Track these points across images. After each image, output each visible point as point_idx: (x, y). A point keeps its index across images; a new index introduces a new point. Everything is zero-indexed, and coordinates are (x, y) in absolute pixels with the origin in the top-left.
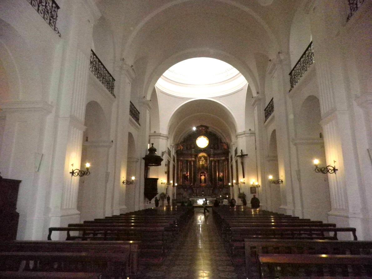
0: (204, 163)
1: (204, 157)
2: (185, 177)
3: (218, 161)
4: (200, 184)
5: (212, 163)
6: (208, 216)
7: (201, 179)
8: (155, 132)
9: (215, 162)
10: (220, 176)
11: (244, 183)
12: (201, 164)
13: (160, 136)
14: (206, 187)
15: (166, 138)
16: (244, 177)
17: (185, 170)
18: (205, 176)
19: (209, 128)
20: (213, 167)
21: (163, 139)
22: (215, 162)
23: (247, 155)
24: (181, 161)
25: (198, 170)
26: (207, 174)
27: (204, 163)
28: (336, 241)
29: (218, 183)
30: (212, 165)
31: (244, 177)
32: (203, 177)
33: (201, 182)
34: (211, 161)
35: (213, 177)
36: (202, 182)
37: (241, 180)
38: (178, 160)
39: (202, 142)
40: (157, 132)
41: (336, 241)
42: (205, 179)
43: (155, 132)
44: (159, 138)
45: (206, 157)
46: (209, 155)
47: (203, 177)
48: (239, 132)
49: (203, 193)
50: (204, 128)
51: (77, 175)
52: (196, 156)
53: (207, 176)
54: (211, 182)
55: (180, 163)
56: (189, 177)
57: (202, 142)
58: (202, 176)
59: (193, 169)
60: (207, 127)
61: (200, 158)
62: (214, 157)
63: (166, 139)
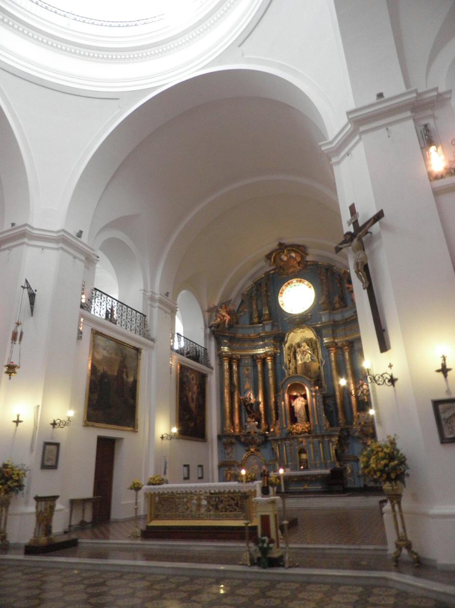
1: (309, 342)
2: (249, 409)
4: (289, 426)
6: (42, 581)
7: (292, 408)
8: (13, 224)
9: (339, 349)
11: (392, 381)
13: (23, 235)
16: (384, 346)
17: (248, 385)
19: (310, 251)
21: (43, 248)
23: (379, 216)
25: (279, 380)
28: (334, 373)
30: (330, 360)
31: (384, 346)
32: (299, 404)
33: (294, 420)
34: (327, 348)
35: (338, 401)
36: (299, 419)
37: (372, 361)
38: (220, 356)
39: (297, 297)
40: (18, 224)
41: (334, 373)
42: (306, 406)
44: (23, 243)
46: (318, 332)
47: (299, 404)
49: (304, 456)
50: (293, 255)
52: (280, 339)
53: (312, 396)
54: (332, 421)
56: (261, 406)
58: (295, 397)
60: (300, 249)
63: (57, 249)
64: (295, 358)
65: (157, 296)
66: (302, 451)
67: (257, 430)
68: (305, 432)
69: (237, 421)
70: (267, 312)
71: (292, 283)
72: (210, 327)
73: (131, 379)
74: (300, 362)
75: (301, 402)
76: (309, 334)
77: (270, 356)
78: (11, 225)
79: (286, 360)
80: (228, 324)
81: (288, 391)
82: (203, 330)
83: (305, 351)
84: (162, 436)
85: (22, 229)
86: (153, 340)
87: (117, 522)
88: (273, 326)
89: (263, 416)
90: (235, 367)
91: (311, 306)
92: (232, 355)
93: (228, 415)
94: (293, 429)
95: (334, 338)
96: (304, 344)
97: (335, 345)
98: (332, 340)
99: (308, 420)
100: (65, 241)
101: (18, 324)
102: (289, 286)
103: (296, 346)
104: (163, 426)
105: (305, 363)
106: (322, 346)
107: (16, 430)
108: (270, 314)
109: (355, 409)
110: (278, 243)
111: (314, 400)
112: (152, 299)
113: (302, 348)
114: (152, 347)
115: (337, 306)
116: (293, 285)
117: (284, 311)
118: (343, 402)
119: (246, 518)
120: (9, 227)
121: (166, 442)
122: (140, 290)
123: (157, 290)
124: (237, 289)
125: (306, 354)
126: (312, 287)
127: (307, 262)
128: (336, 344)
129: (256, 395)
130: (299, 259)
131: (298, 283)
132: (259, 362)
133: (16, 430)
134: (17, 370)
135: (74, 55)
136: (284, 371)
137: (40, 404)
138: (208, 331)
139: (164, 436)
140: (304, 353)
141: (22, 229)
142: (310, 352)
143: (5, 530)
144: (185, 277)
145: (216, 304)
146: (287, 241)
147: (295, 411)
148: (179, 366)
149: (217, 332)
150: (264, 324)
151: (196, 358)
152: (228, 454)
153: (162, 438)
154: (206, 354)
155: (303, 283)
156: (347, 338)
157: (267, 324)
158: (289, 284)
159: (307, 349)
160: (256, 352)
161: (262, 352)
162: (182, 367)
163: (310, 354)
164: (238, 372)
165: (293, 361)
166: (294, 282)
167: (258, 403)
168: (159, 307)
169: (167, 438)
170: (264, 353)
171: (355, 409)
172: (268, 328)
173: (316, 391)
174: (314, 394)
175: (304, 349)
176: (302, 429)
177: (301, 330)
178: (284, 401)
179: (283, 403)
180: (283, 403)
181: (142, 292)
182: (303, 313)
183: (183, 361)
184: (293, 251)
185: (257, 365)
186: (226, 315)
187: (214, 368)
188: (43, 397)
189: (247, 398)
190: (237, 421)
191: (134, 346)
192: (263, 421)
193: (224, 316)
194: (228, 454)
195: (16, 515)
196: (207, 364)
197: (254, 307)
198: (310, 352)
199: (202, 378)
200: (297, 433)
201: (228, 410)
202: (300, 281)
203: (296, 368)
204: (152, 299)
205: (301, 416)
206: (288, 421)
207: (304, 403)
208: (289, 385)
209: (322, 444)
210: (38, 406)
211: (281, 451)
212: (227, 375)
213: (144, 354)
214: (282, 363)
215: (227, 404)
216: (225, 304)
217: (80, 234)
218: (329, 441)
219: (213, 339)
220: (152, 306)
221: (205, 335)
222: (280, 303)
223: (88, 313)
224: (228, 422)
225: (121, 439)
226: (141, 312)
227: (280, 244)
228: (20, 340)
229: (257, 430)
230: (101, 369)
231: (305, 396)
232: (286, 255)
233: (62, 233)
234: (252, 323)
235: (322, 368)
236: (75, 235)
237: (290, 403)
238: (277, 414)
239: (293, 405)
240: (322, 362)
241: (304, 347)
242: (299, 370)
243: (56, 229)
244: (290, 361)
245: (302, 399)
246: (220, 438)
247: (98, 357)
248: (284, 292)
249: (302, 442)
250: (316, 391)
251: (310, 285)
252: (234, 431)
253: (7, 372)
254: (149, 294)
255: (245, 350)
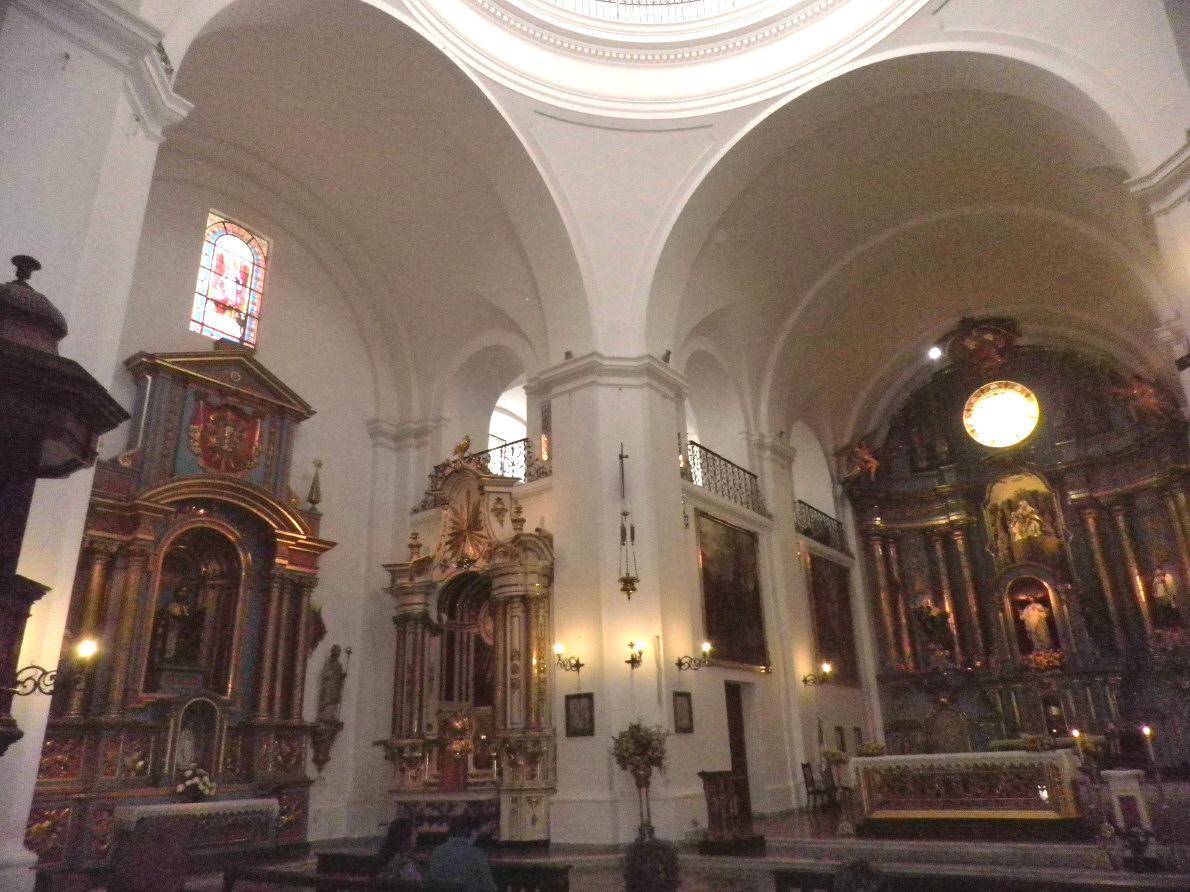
0: (1034, 529)
2: (930, 628)
3: (1128, 500)
4: (1020, 658)
5: (1083, 521)
7: (1021, 625)
8: (568, 355)
9: (1104, 511)
10: (1160, 592)
12: (1018, 537)
14: (1065, 670)
15: (645, 380)
18: (1045, 602)
19: (1023, 326)
20: (1095, 542)
22: (1104, 511)
24: (885, 538)
25: (990, 579)
26: (1055, 590)
27: (1034, 529)
29: (1159, 637)
30: (1086, 530)
32: (1034, 615)
34: (1079, 507)
36: (1037, 645)
38: (865, 535)
42: (1050, 621)
43: (568, 355)
45: (1047, 499)
46: (1056, 480)
47: (1034, 615)
48: (1157, 163)
50: (989, 337)
51: (34, 690)
52: (975, 498)
53: (1060, 602)
55: (885, 550)
56: (951, 620)
57: (1003, 417)
58: (1025, 604)
59: (967, 573)
60: (1005, 326)
61: (1011, 505)
62: (1089, 484)
63: (641, 386)
64: (1006, 529)
65: (768, 441)
66: (1049, 701)
67: (951, 665)
68: (1054, 667)
69: (908, 650)
70: (946, 448)
71: (988, 389)
72: (843, 484)
73: (751, 586)
74: (1018, 537)
75: (1037, 612)
76: (1033, 483)
77: (960, 528)
78: (564, 356)
79: (990, 531)
80: (876, 474)
81: (1009, 593)
82: (831, 489)
83: (1027, 516)
84: (680, 661)
85: (589, 360)
86: (770, 517)
87: (763, 817)
88: (959, 471)
89: (956, 639)
90: (892, 552)
91: (1036, 428)
92: (887, 530)
93: (891, 638)
94: (1030, 661)
95: (1091, 490)
96: (1023, 503)
97: (1093, 503)
98: (1087, 494)
99: (1055, 644)
100: (652, 372)
101: (625, 514)
102: (983, 397)
103: (1006, 507)
104: (800, 662)
105: (1030, 538)
106: (1064, 506)
107: (632, 675)
108: (952, 451)
109: (1148, 624)
110: (958, 319)
111: (1065, 608)
112: (761, 446)
113: (1020, 510)
114: (771, 530)
115: (1093, 428)
116: (991, 392)
117: (981, 446)
118: (1120, 608)
119: (1058, 810)
120: (561, 358)
121: (811, 689)
122: (740, 433)
123: (765, 429)
124: (882, 406)
125: (1030, 523)
126: (1032, 395)
127: (1018, 347)
128: (1096, 500)
129: (938, 600)
130: (1001, 345)
131: (1003, 390)
132: (937, 540)
133: (632, 675)
134: (636, 585)
135: (601, 61)
136: (989, 555)
137: (660, 634)
138: (839, 489)
139: (684, 661)
140: (1025, 520)
141: (589, 360)
142: (1037, 518)
143: (649, 822)
144: (800, 405)
145: (846, 440)
146: (979, 313)
147: (1028, 629)
148: (809, 559)
149: (857, 492)
150: (941, 471)
151: (824, 538)
152: (901, 707)
153: (805, 681)
154: (841, 533)
155: (1012, 387)
156: (1119, 490)
157: (949, 470)
158: (982, 392)
159: (1032, 512)
160: (936, 523)
161: (944, 522)
162: (814, 559)
163: (1037, 521)
164: (900, 561)
165: (1001, 534)
166: (992, 387)
167: (945, 616)
168: (773, 460)
169: (689, 666)
170: (946, 523)
171: (1148, 624)
172: (951, 478)
173: (1067, 592)
174: (1063, 597)
175: (1025, 513)
176: (1048, 662)
177: (1016, 477)
178: (1003, 610)
179: (1001, 615)
180: (1001, 615)
181: (744, 435)
182: (1018, 444)
183: (815, 549)
184: (988, 330)
185: (933, 547)
186: (872, 459)
187: (856, 556)
188: (663, 625)
189: (922, 607)
190: (908, 650)
191: (747, 529)
192: (957, 649)
193: (867, 462)
194: (901, 707)
195: (659, 800)
196: (843, 547)
197: (916, 439)
198: (1037, 518)
199: (843, 574)
200: (1038, 669)
201: (890, 630)
202: (1006, 386)
203: (1010, 548)
204: (761, 446)
205: (1041, 638)
206: (1016, 648)
207: (1044, 615)
208: (1010, 584)
209: (1091, 689)
210: (658, 637)
211: (1007, 703)
212: (880, 568)
213: (763, 541)
214: (984, 540)
215: (888, 621)
216: (864, 439)
217: (666, 358)
218: (1105, 683)
219: (848, 503)
220: (761, 458)
221: (835, 498)
222: (968, 430)
223: (689, 483)
224: (893, 652)
225: (750, 685)
226: (747, 469)
227: (964, 321)
228: (633, 538)
229: (951, 665)
230: (712, 569)
231: (1045, 602)
232: (975, 339)
233: (647, 361)
234: (916, 470)
235: (1068, 548)
236: (660, 359)
237: (1016, 615)
238: (986, 634)
239: (1021, 617)
240: (1067, 537)
241: (1025, 509)
242: (1017, 555)
243: (634, 354)
244: (996, 536)
245: (1039, 606)
246: (879, 679)
247: (709, 554)
248: (974, 408)
249: (1049, 684)
250: (1067, 592)
251: (1028, 391)
252: (907, 668)
253: (623, 590)
254: (755, 438)
255: (910, 519)
